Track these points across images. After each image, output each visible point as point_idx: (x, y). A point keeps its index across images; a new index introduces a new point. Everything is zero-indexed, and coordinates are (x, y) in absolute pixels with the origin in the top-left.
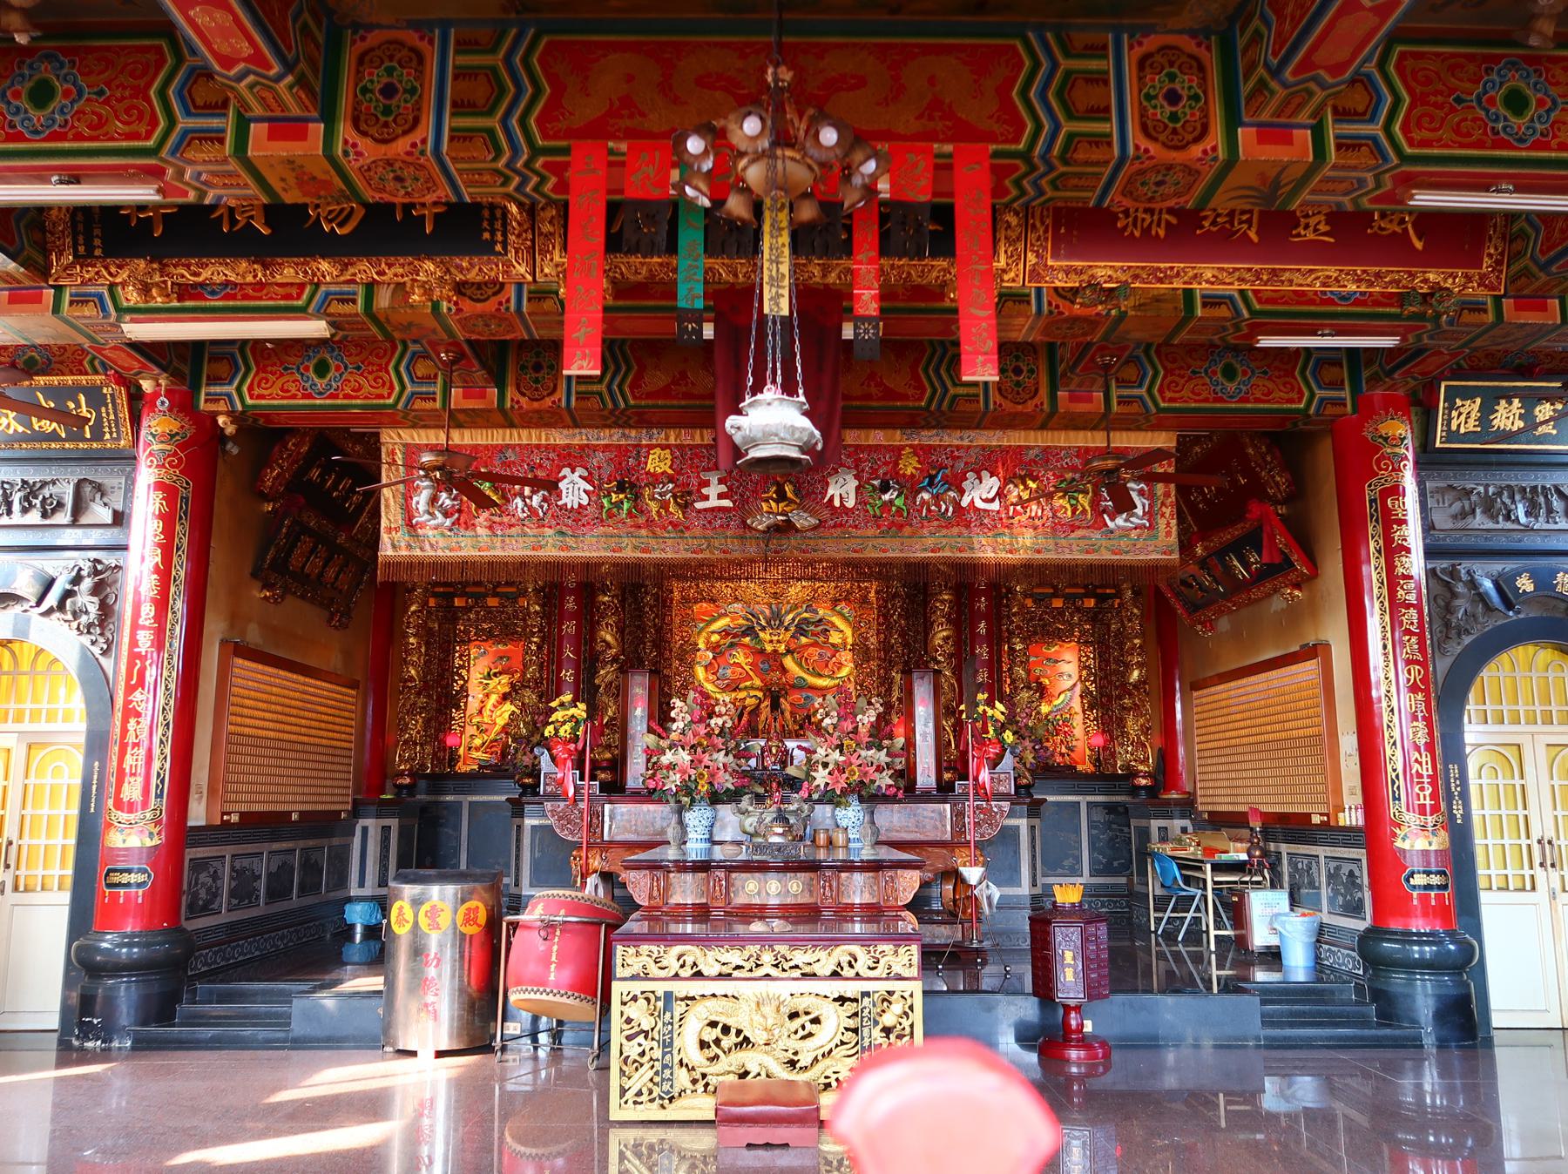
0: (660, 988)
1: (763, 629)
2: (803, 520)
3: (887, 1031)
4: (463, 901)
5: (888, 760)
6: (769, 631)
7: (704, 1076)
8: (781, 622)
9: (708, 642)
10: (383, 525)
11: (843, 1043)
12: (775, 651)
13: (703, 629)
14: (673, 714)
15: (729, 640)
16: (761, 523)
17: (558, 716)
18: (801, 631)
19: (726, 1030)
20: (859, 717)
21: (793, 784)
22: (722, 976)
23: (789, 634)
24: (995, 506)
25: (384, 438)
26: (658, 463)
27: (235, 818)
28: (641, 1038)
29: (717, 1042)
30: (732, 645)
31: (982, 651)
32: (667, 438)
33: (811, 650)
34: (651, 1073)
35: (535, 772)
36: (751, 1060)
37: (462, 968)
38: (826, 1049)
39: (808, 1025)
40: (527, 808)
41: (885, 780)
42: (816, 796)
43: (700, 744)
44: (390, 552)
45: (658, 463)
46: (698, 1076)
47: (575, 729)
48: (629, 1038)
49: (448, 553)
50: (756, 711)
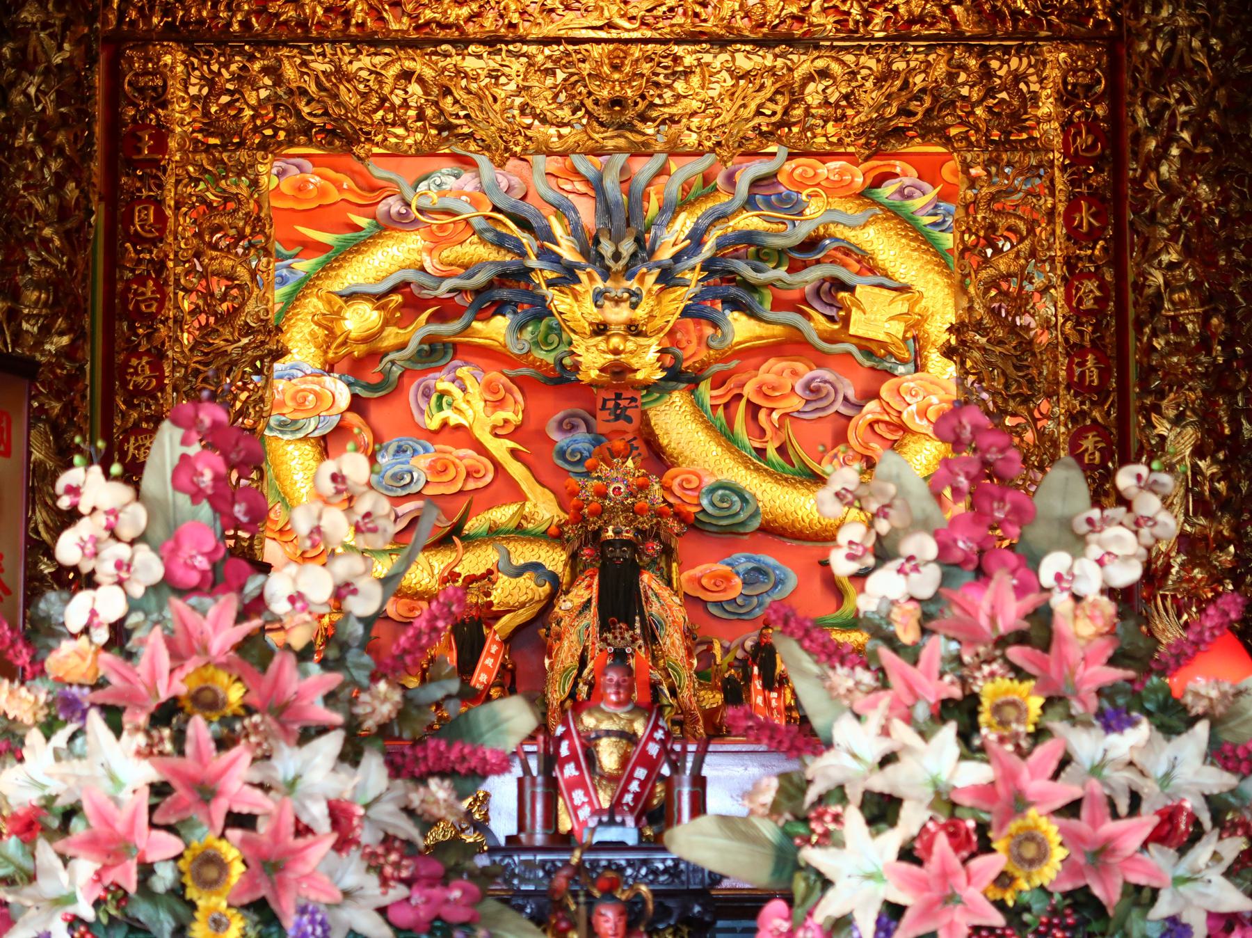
5: (1218, 780)
6: (590, 282)
9: (329, 323)
12: (618, 371)
13: (307, 284)
14: (68, 549)
15: (420, 328)
18: (728, 286)
20: (1052, 565)
23: (678, 299)
30: (434, 353)
33: (772, 370)
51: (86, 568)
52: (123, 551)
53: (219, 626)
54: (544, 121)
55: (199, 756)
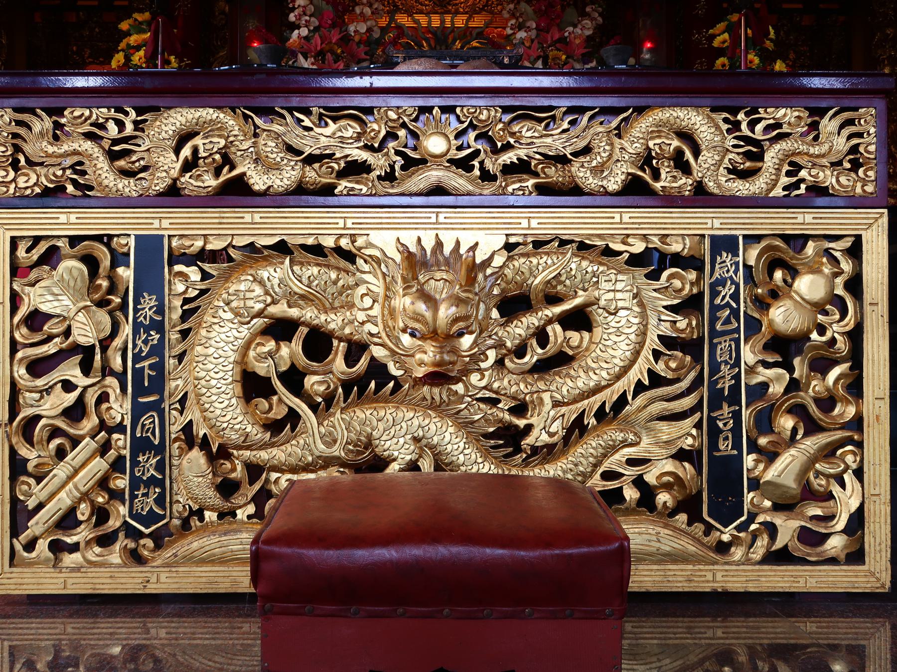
0: (128, 226)
3: (783, 347)
7: (254, 470)
11: (656, 380)
14: (292, 17)
19: (318, 344)
22: (300, 192)
28: (71, 371)
29: (293, 379)
34: (99, 465)
36: (397, 431)
38: (610, 396)
39: (555, 331)
46: (239, 473)
48: (37, 367)
51: (297, 23)
52: (307, 18)
53: (335, 36)
54: (422, 5)
55: (329, 64)
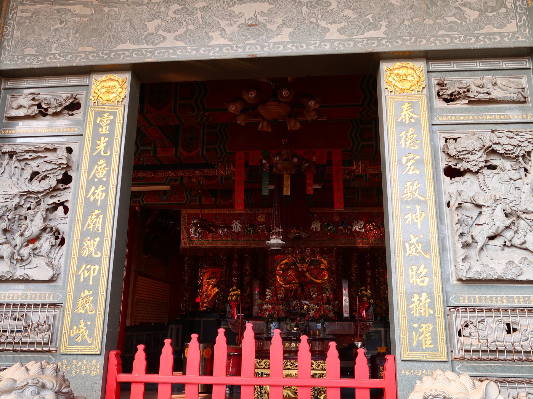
1: (298, 263)
2: (304, 235)
4: (205, 349)
8: (305, 261)
9: (280, 266)
10: (182, 237)
12: (303, 271)
13: (279, 263)
16: (292, 236)
17: (232, 293)
21: (304, 315)
24: (363, 231)
25: (182, 212)
26: (261, 218)
27: (137, 324)
31: (369, 272)
32: (264, 211)
35: (225, 311)
37: (204, 368)
40: (222, 323)
41: (331, 315)
42: (310, 319)
43: (275, 303)
44: (183, 246)
45: (261, 218)
47: (237, 298)
49: (200, 246)
50: (296, 291)
